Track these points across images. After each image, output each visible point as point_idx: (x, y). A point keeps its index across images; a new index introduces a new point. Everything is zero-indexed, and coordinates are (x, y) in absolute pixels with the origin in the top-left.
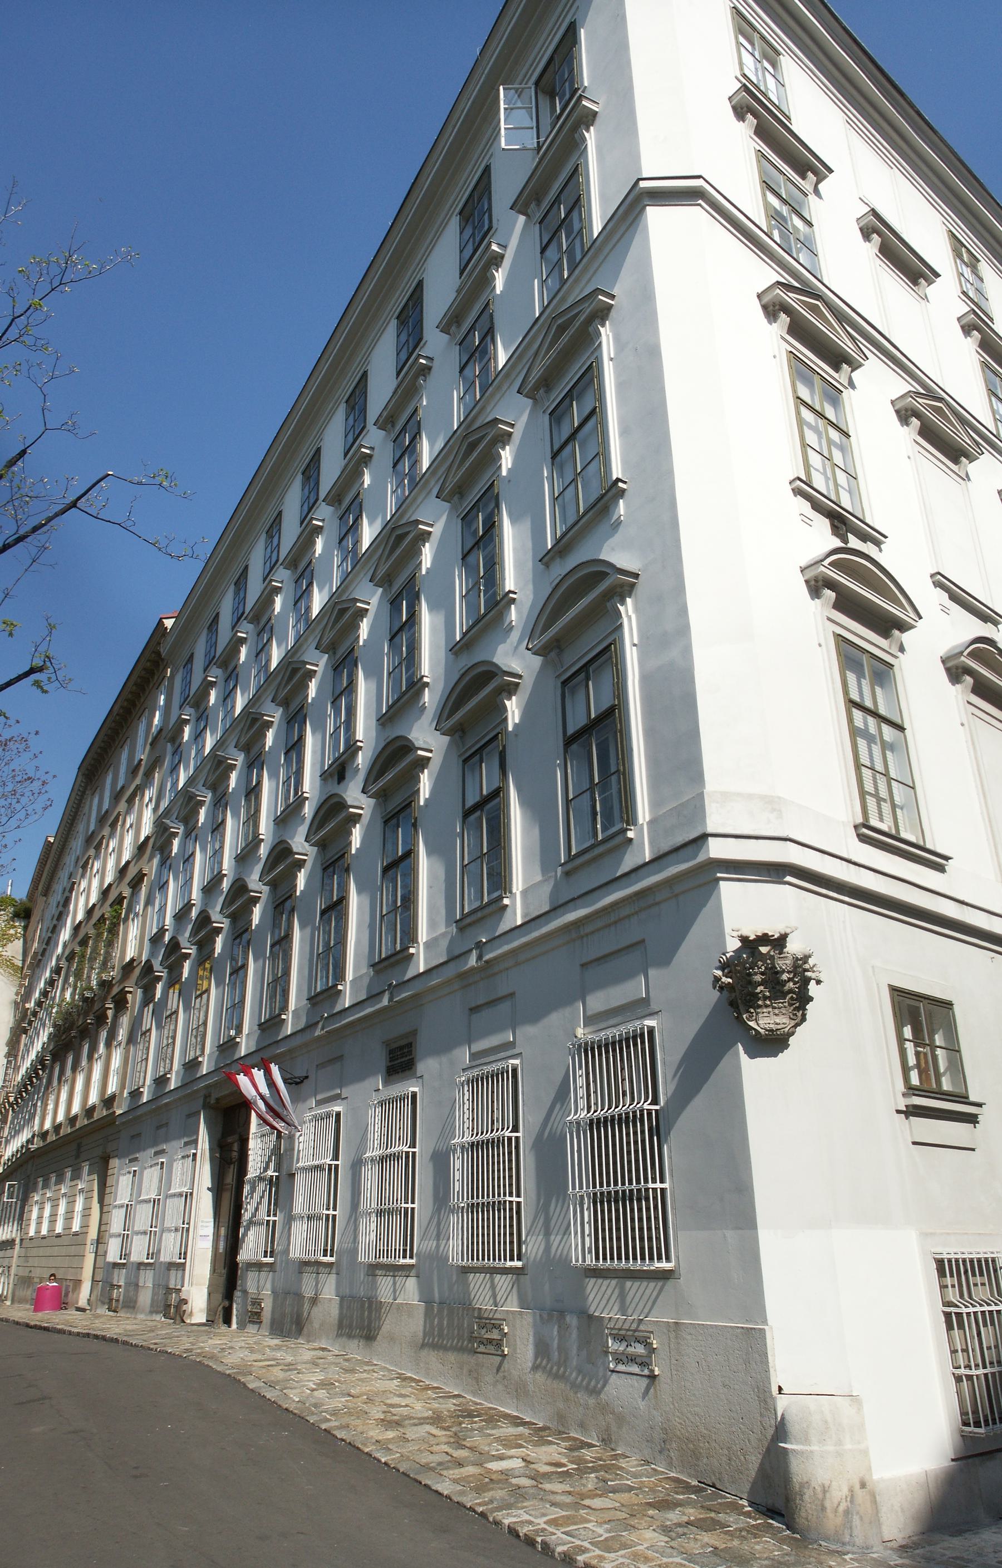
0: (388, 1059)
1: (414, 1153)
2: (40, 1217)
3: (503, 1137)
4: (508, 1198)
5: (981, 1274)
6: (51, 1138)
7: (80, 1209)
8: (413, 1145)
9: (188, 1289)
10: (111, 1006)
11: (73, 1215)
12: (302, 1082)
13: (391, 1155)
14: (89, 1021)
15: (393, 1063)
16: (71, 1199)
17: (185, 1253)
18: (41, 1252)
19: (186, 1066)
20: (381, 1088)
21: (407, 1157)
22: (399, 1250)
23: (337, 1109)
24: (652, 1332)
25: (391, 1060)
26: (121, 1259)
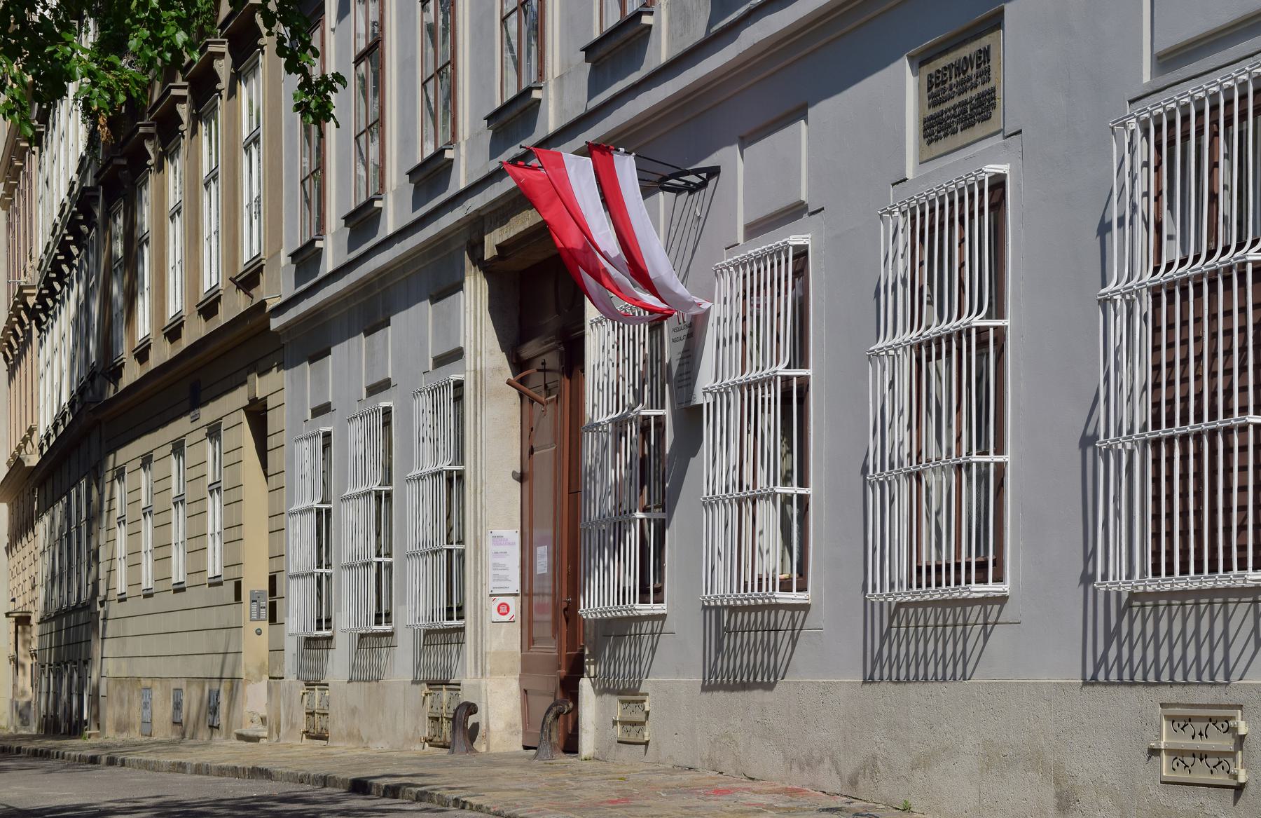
0: (926, 101)
1: (1000, 332)
2: (134, 553)
3: (1244, 265)
4: (975, 458)
5: (1107, 594)
6: (196, 330)
7: (150, 547)
8: (997, 310)
9: (474, 682)
10: (185, 92)
11: (205, 542)
12: (704, 184)
13: (960, 333)
14: (141, 130)
15: (938, 110)
16: (195, 508)
17: (460, 609)
18: (148, 624)
19: (419, 177)
20: (909, 174)
21: (982, 344)
22: (968, 565)
23: (796, 240)
24: (1240, 707)
25: (935, 101)
26: (319, 628)
